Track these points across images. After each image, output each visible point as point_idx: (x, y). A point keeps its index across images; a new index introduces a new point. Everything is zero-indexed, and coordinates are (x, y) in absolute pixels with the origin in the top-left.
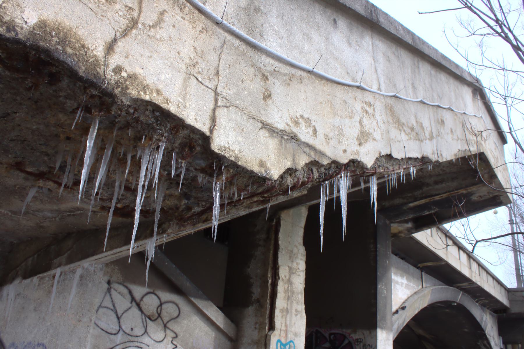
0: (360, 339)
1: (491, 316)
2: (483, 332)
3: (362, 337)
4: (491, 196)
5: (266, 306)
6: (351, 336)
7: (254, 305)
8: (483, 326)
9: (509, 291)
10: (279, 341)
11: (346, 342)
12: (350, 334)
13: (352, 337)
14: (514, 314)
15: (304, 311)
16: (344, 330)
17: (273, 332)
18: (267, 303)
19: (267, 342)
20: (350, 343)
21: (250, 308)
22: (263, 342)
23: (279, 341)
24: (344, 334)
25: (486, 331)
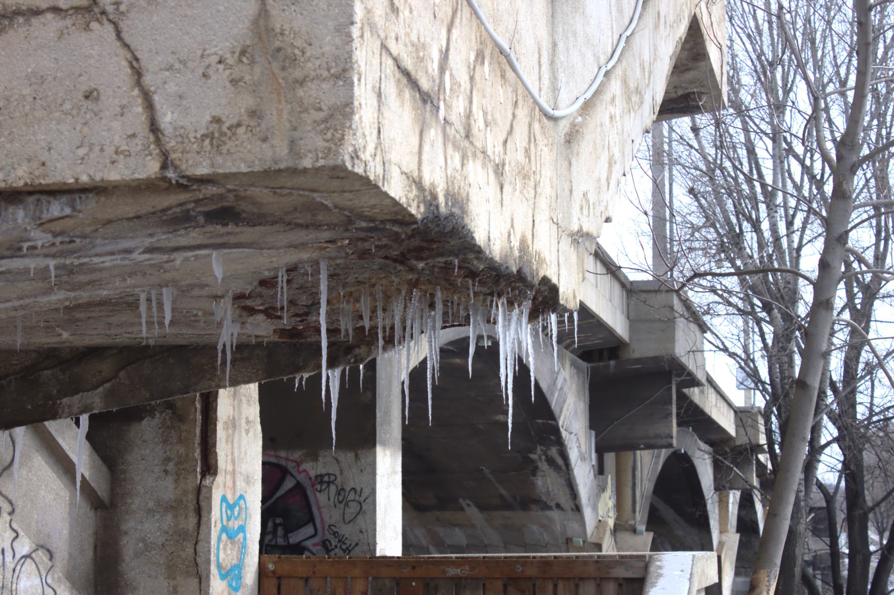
0: (329, 475)
1: (574, 371)
2: (553, 422)
3: (333, 469)
4: (680, 93)
5: (191, 417)
6: (301, 469)
7: (158, 415)
8: (553, 405)
9: (630, 290)
10: (224, 499)
11: (289, 484)
12: (298, 464)
13: (305, 471)
14: (638, 361)
15: (258, 420)
16: (283, 454)
17: (214, 480)
18: (196, 409)
19: (203, 504)
20: (299, 486)
21: (144, 422)
22: (192, 506)
23: (224, 499)
24: (283, 463)
25: (559, 417)
